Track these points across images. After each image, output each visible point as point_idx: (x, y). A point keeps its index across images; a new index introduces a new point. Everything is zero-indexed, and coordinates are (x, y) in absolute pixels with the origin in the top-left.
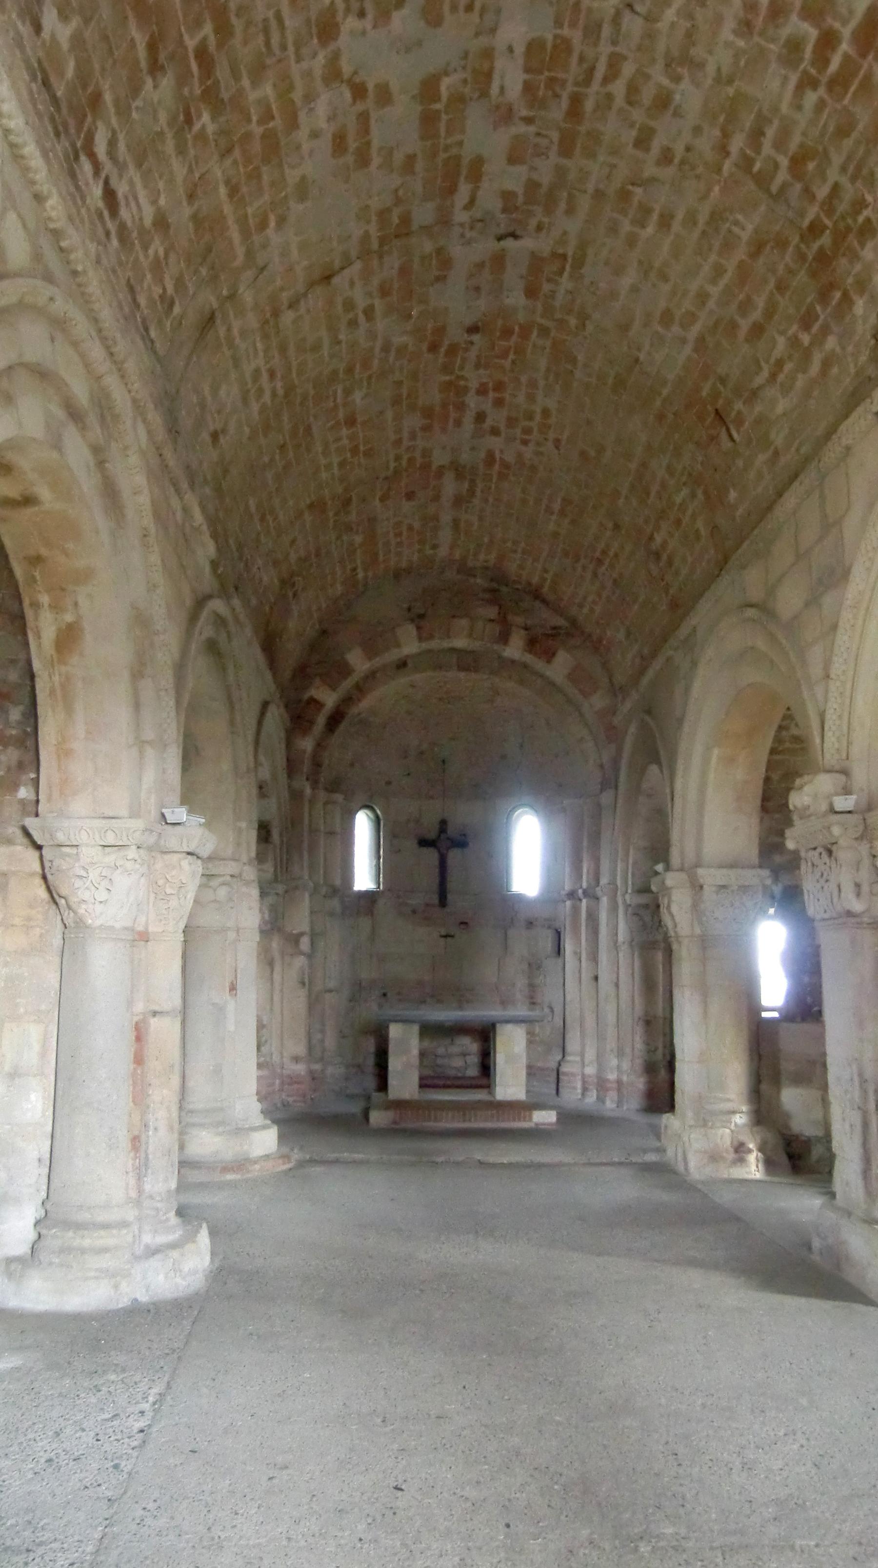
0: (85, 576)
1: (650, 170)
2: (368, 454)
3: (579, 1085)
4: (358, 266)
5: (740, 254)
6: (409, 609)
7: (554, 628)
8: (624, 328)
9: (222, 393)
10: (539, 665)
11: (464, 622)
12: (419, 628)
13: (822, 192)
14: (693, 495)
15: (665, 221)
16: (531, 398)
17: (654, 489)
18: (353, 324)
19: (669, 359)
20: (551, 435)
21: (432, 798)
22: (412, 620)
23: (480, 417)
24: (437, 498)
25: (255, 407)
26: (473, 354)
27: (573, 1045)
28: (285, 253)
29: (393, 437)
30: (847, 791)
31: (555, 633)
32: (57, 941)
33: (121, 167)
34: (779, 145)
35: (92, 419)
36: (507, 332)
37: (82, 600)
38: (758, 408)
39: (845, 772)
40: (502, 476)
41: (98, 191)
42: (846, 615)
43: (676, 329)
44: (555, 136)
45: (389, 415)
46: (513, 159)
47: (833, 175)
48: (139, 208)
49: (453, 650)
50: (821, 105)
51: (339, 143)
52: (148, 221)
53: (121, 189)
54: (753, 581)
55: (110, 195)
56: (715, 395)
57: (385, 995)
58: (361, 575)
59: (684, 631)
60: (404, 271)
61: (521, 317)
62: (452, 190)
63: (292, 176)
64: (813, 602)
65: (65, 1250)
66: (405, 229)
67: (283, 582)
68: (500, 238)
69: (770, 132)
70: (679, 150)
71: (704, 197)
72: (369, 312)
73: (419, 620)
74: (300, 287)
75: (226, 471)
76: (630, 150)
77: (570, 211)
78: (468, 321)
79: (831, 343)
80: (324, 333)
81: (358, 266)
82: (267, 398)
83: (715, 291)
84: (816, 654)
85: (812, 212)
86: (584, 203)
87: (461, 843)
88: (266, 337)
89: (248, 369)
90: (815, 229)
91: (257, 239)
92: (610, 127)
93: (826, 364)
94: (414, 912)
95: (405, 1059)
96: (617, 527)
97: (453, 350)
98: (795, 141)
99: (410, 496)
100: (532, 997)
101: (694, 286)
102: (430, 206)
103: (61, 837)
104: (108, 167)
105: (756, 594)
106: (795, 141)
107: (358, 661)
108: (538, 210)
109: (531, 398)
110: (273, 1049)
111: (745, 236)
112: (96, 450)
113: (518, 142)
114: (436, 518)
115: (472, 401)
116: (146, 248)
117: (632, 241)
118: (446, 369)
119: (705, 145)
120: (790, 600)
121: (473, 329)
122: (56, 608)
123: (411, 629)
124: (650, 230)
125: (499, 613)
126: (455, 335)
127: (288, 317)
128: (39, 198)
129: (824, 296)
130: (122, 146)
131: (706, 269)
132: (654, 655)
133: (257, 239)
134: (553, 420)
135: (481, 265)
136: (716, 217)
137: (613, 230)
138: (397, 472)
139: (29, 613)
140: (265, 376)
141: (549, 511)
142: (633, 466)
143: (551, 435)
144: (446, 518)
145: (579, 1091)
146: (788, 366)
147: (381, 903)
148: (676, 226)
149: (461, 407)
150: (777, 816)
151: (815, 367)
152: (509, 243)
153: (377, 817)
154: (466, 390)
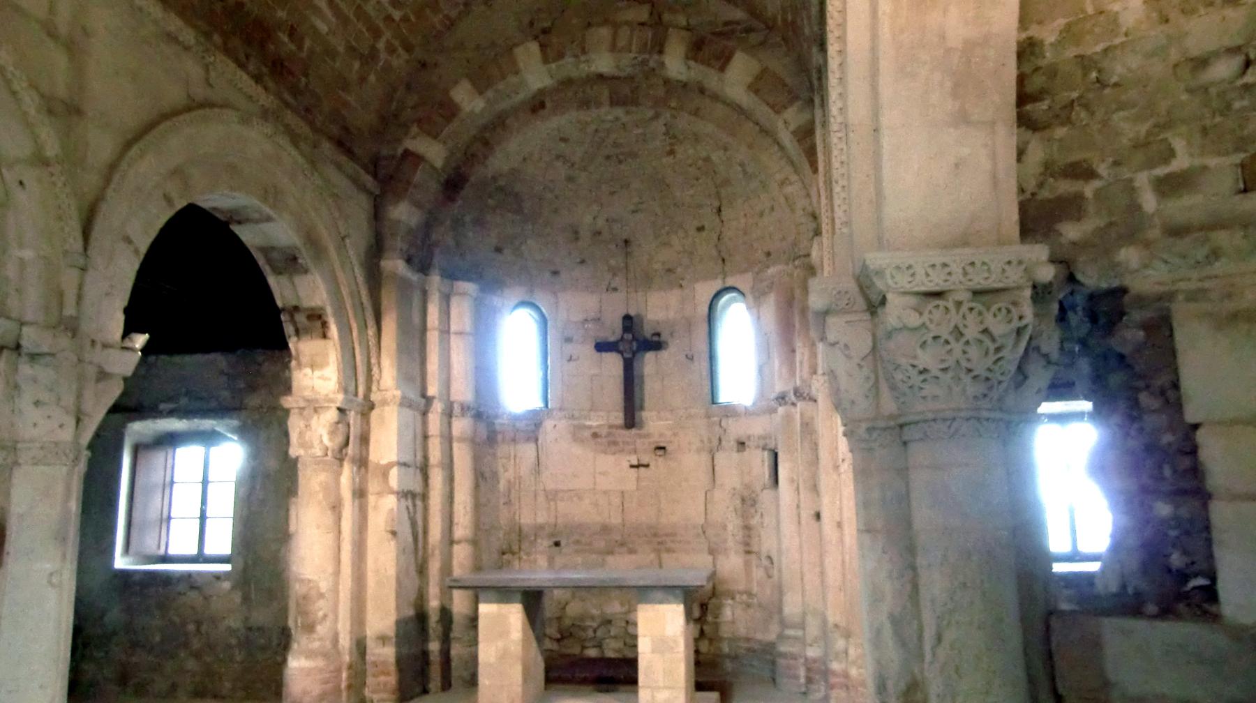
3: (802, 672)
6: (531, 24)
7: (727, 23)
10: (712, 79)
11: (604, 32)
12: (543, 47)
21: (615, 289)
22: (536, 38)
31: (728, 32)
57: (557, 544)
87: (655, 344)
94: (595, 435)
95: (500, 644)
100: (747, 544)
107: (469, 101)
110: (340, 626)
123: (534, 47)
125: (651, 14)
145: (802, 680)
147: (548, 424)
150: (1060, 132)
153: (542, 316)
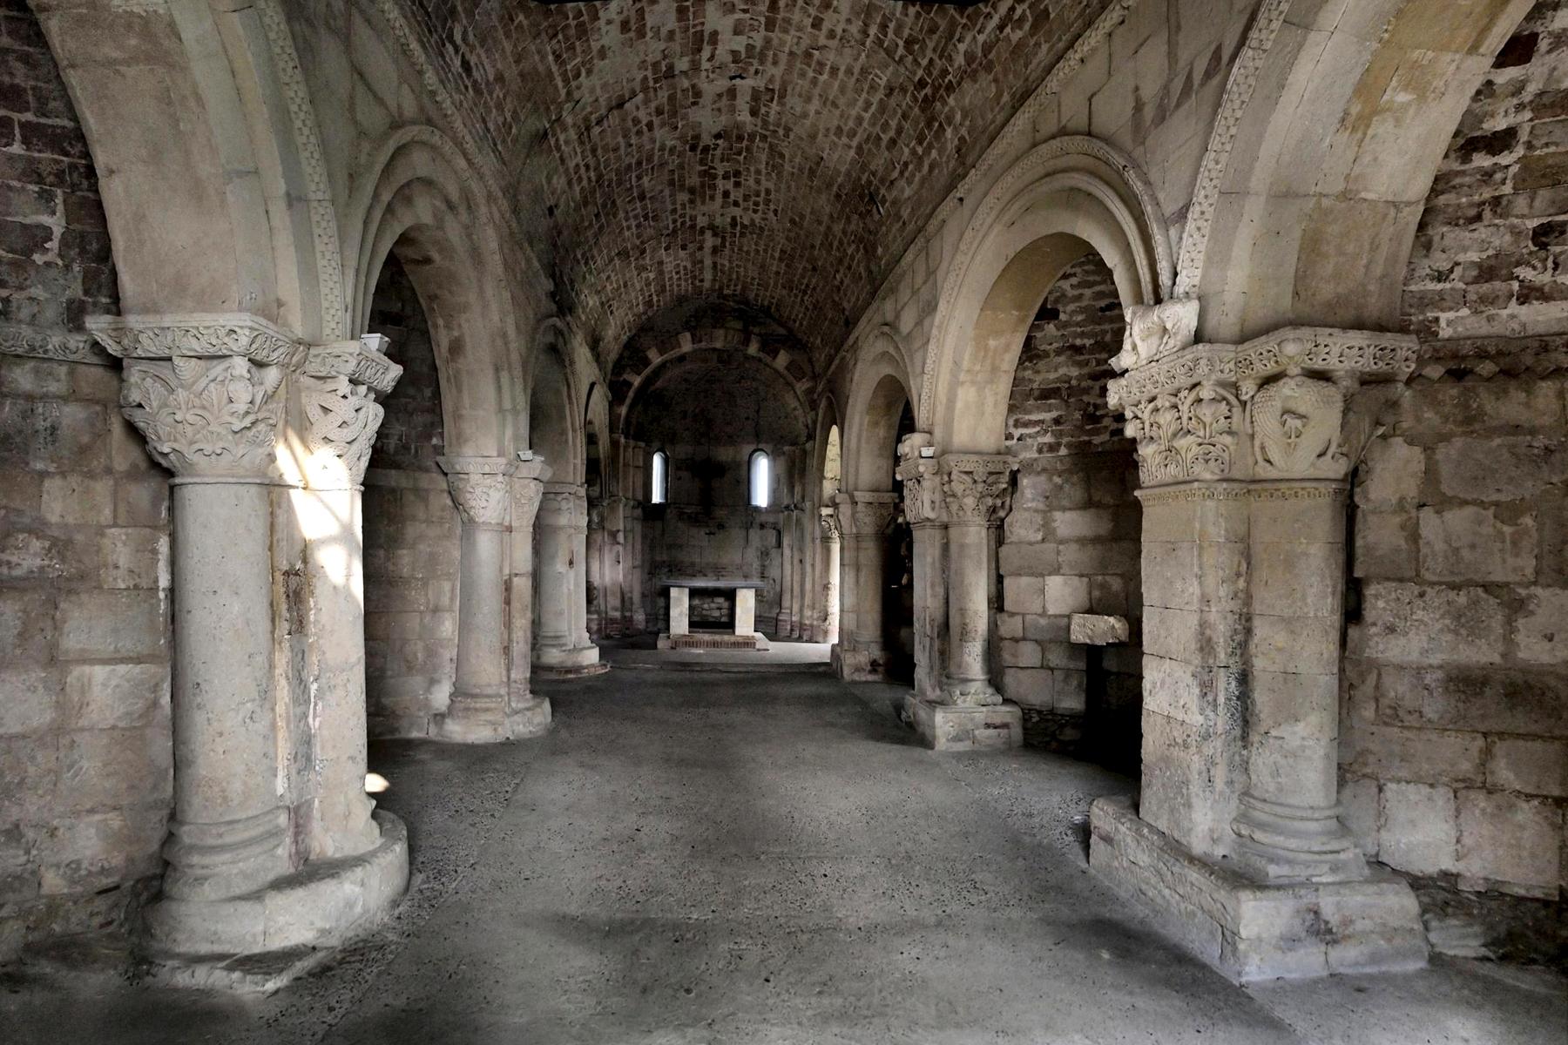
0: (465, 308)
1: (822, 41)
2: (655, 218)
4: (641, 96)
5: (880, 94)
8: (813, 137)
9: (555, 180)
10: (768, 359)
11: (722, 332)
13: (924, 62)
14: (858, 250)
15: (834, 71)
16: (758, 182)
17: (836, 244)
18: (639, 133)
19: (840, 157)
20: (772, 207)
23: (726, 194)
24: (701, 248)
25: (577, 189)
26: (718, 152)
27: (786, 603)
28: (592, 90)
29: (670, 207)
30: (930, 445)
32: (459, 531)
33: (472, 49)
34: (897, 32)
35: (462, 209)
36: (740, 138)
37: (465, 326)
38: (894, 193)
39: (930, 433)
40: (742, 234)
41: (458, 62)
42: (935, 332)
43: (845, 140)
44: (763, 20)
45: (667, 192)
46: (737, 31)
47: (929, 54)
48: (486, 68)
49: (715, 349)
50: (918, 15)
51: (625, 26)
52: (491, 78)
53: (473, 60)
54: (888, 307)
55: (466, 65)
56: (870, 183)
58: (655, 298)
59: (851, 341)
60: (672, 98)
61: (749, 128)
62: (700, 50)
63: (595, 46)
64: (919, 323)
65: (467, 709)
66: (670, 74)
67: (602, 304)
68: (732, 78)
69: (892, 26)
70: (839, 31)
71: (856, 60)
72: (650, 126)
73: (692, 330)
74: (603, 111)
75: (559, 233)
76: (809, 29)
77: (775, 63)
78: (715, 131)
79: (934, 153)
80: (620, 139)
81: (641, 96)
82: (585, 183)
83: (867, 116)
84: (918, 357)
85: (920, 73)
86: (783, 58)
88: (582, 143)
89: (572, 165)
90: (921, 84)
91: (574, 84)
92: (796, 16)
93: (932, 168)
96: (814, 269)
97: (706, 149)
98: (906, 32)
99: (684, 247)
101: (854, 113)
102: (686, 59)
103: (458, 468)
104: (463, 48)
105: (889, 317)
106: (906, 32)
107: (656, 358)
108: (755, 62)
109: (758, 182)
111: (883, 82)
112: (467, 227)
113: (738, 23)
114: (702, 262)
115: (720, 183)
116: (491, 94)
117: (814, 82)
118: (702, 162)
119: (854, 29)
120: (907, 323)
121: (718, 136)
122: (448, 327)
124: (825, 76)
126: (706, 140)
127: (596, 130)
128: (421, 73)
129: (929, 125)
130: (471, 37)
131: (860, 103)
132: (837, 352)
133: (574, 84)
134: (772, 197)
135: (720, 96)
136: (864, 71)
137: (803, 75)
138: (675, 231)
139: (432, 331)
140: (583, 170)
141: (772, 257)
142: (822, 229)
143: (772, 207)
144: (708, 262)
146: (911, 167)
148: (841, 74)
149: (713, 187)
151: (926, 168)
152: (738, 81)
154: (715, 177)
